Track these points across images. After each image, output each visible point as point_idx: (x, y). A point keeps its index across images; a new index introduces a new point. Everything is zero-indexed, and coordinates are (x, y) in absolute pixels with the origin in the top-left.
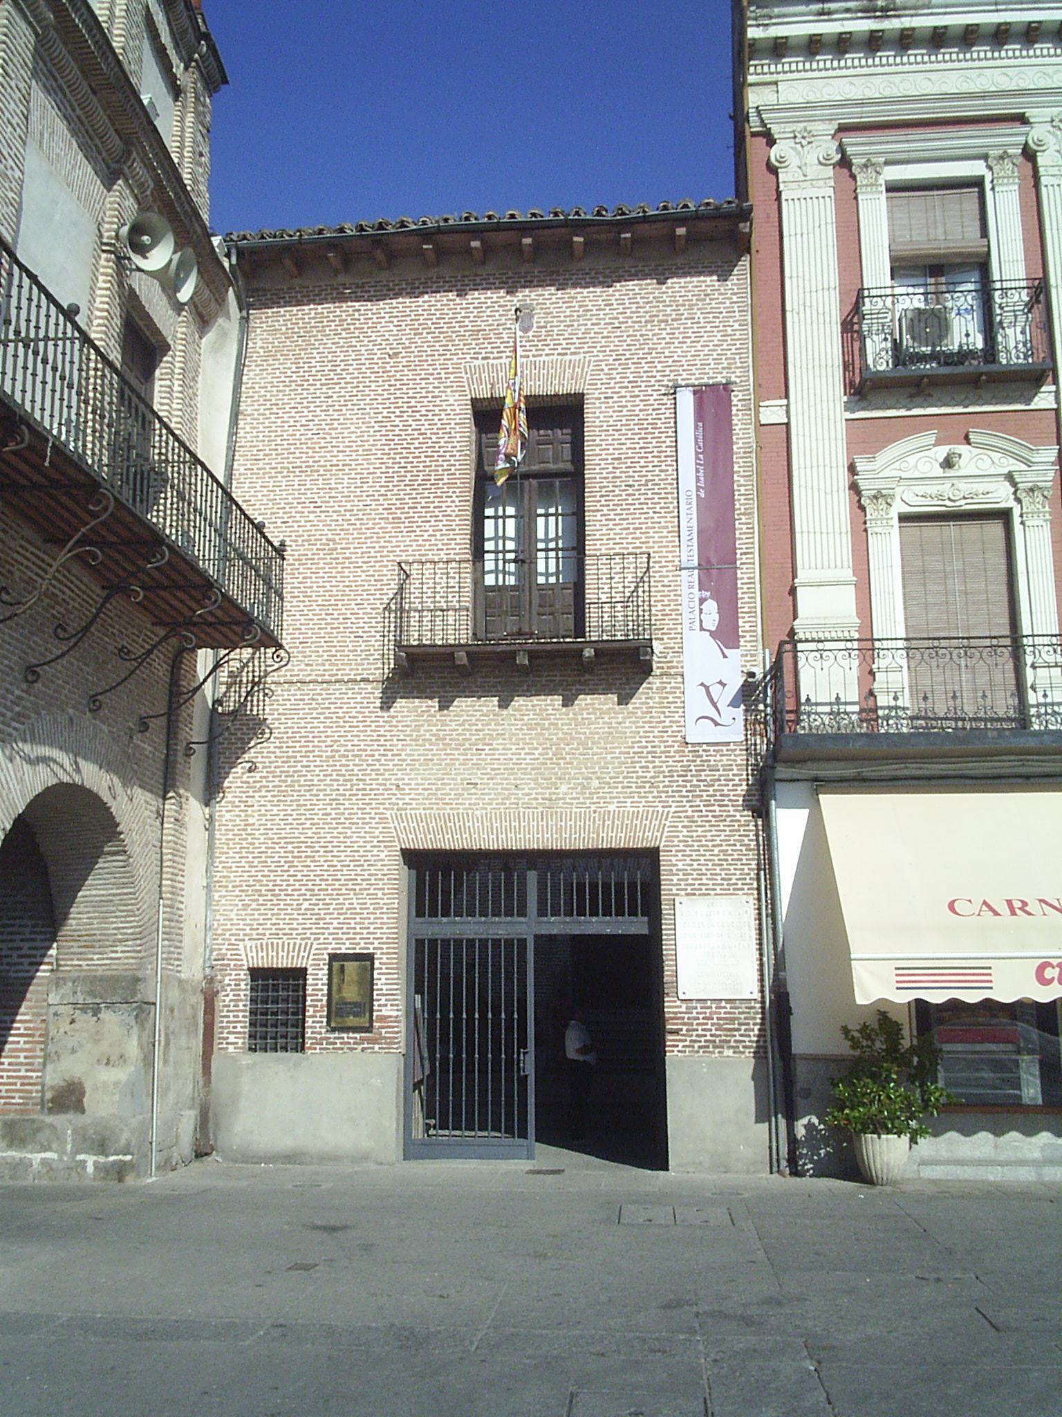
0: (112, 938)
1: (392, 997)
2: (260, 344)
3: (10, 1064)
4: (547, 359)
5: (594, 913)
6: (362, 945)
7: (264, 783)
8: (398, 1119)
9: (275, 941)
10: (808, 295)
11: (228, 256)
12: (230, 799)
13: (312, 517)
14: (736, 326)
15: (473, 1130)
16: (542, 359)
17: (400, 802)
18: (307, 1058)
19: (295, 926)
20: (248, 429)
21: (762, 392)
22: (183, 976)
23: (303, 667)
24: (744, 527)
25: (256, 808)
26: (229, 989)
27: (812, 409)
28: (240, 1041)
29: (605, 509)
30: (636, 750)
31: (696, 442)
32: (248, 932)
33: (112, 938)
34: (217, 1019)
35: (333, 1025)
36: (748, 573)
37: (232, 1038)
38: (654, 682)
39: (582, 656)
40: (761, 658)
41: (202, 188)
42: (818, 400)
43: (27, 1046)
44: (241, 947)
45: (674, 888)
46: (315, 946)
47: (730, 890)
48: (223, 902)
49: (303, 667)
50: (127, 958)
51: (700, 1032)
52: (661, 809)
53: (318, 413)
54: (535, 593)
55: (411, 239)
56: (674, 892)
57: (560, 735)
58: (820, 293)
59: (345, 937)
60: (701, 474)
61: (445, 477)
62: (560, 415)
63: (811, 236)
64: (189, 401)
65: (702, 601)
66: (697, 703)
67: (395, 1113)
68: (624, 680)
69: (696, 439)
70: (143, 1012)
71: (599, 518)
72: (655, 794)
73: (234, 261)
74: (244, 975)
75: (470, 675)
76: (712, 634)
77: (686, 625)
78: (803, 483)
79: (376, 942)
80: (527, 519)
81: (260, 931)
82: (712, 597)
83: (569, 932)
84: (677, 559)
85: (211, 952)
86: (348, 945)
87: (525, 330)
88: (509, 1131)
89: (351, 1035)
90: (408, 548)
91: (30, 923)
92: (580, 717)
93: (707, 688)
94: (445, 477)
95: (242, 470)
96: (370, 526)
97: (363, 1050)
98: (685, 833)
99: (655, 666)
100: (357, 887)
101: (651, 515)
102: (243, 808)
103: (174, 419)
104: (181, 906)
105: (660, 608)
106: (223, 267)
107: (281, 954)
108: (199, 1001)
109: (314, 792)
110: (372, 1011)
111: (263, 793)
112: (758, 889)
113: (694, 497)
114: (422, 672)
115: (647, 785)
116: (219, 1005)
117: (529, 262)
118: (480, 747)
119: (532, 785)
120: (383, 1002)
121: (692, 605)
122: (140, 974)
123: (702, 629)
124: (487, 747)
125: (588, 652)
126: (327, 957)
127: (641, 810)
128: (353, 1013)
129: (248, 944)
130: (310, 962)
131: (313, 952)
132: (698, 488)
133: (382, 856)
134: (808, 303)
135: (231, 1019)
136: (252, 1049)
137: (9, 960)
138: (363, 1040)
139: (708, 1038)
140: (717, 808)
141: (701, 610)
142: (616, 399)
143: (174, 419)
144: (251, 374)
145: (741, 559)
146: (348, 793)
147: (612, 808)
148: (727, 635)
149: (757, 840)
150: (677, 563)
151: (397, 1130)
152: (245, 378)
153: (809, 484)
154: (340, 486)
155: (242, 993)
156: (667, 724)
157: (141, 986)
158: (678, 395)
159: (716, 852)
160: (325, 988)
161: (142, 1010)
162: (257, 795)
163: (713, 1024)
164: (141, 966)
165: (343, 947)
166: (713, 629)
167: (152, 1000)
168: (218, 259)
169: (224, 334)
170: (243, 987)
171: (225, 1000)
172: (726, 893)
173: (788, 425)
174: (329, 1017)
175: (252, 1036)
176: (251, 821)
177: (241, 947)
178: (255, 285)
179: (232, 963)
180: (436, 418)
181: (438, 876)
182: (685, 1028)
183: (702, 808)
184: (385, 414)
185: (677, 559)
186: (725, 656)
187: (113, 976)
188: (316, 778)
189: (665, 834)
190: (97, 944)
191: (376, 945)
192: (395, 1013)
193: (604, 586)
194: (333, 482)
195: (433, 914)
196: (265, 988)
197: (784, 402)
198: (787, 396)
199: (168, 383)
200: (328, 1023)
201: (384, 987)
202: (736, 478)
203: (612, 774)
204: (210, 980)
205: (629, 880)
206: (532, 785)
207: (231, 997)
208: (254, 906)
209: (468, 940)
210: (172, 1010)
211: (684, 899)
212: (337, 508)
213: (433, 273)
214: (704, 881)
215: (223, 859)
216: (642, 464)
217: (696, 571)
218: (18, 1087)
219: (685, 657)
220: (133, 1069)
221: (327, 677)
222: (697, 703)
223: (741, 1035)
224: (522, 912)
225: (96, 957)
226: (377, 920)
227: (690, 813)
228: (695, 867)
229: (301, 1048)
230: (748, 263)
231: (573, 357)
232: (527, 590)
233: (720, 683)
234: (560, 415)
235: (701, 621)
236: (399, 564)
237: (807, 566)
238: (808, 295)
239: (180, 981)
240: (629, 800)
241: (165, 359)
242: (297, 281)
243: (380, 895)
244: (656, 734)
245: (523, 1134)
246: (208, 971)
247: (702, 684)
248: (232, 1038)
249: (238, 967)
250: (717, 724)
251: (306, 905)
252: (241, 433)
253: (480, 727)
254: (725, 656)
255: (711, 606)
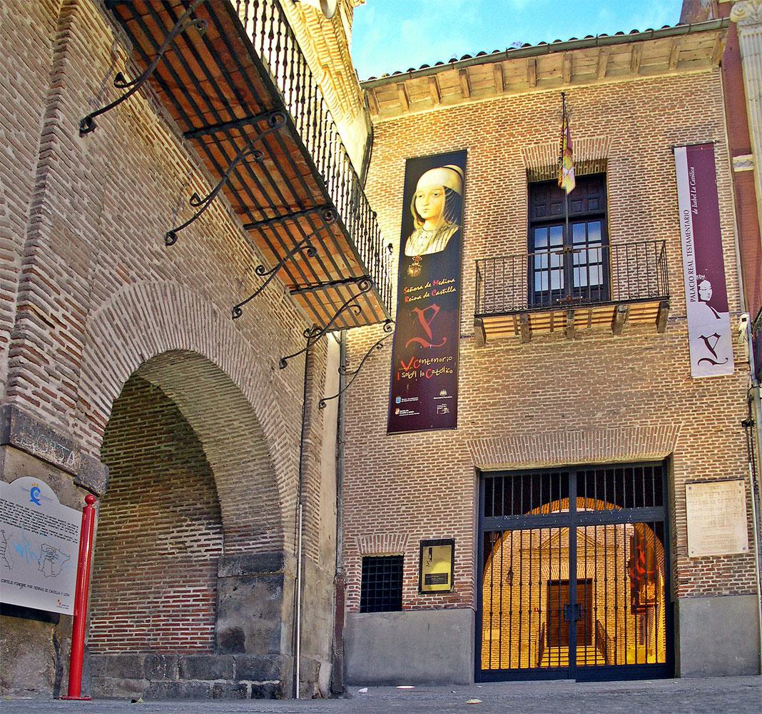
3: (193, 620)
31: (690, 180)
32: (361, 529)
43: (204, 608)
44: (356, 540)
46: (410, 537)
51: (705, 580)
52: (673, 425)
60: (695, 199)
65: (699, 282)
69: (690, 177)
76: (708, 303)
77: (688, 299)
79: (456, 531)
84: (679, 257)
86: (434, 535)
91: (205, 522)
93: (706, 340)
118: (536, 391)
121: (692, 284)
123: (700, 300)
129: (361, 537)
131: (408, 540)
132: (693, 209)
133: (461, 471)
137: (191, 549)
139: (711, 583)
141: (699, 288)
156: (677, 366)
160: (418, 565)
162: (369, 436)
163: (713, 574)
177: (356, 540)
179: (349, 551)
180: (502, 182)
182: (692, 578)
185: (679, 257)
186: (718, 317)
201: (462, 562)
208: (365, 511)
218: (199, 636)
223: (735, 580)
231: (599, 137)
233: (716, 335)
235: (699, 295)
243: (459, 498)
247: (702, 337)
250: (714, 363)
251: (403, 508)
255: (706, 285)
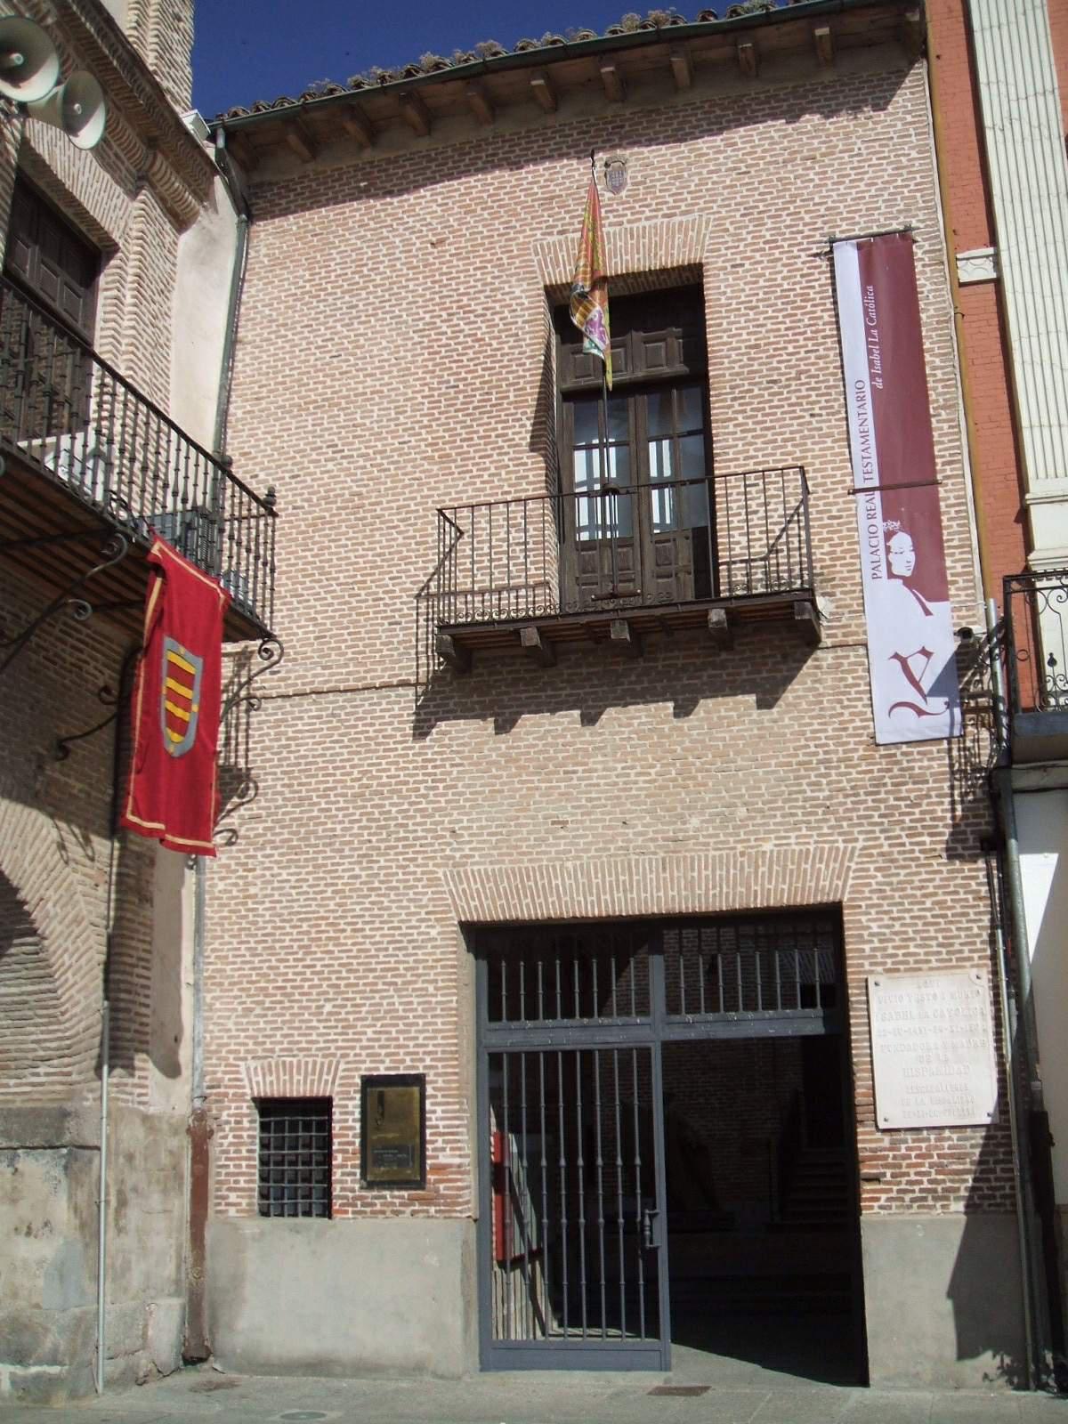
0: (30, 1055)
1: (453, 1134)
2: (264, 251)
4: (647, 224)
5: (750, 1005)
6: (408, 1063)
7: (269, 837)
8: (466, 1313)
9: (288, 1059)
10: (1014, 105)
11: (212, 138)
12: (224, 861)
13: (330, 466)
14: (914, 154)
15: (580, 1325)
16: (640, 224)
17: (458, 855)
18: (334, 1226)
19: (314, 1038)
20: (248, 361)
21: (955, 239)
22: (152, 1110)
23: (319, 670)
24: (945, 426)
25: (258, 872)
26: (227, 1128)
27: (1033, 255)
28: (244, 1202)
29: (740, 417)
30: (801, 758)
31: (866, 313)
32: (251, 1047)
33: (30, 1055)
34: (213, 1170)
35: (369, 1178)
36: (955, 491)
37: (233, 1197)
38: (825, 658)
39: (707, 622)
40: (982, 611)
41: (179, 58)
42: (1041, 243)
45: (866, 963)
46: (342, 1066)
47: (952, 961)
48: (218, 1005)
49: (319, 670)
50: (52, 1083)
52: (841, 845)
53: (339, 328)
54: (649, 547)
55: (451, 86)
56: (867, 967)
57: (687, 744)
58: (1032, 100)
59: (383, 1052)
60: (876, 357)
61: (511, 395)
62: (666, 304)
63: (1013, 27)
64: (154, 323)
65: (889, 535)
66: (888, 685)
67: (460, 1304)
68: (779, 658)
70: (76, 1160)
71: (731, 429)
72: (833, 823)
73: (221, 142)
74: (247, 1108)
75: (554, 665)
76: (908, 582)
77: (867, 572)
78: (1027, 357)
80: (633, 446)
81: (268, 1046)
82: (903, 529)
83: (712, 1035)
84: (848, 479)
85: (203, 1076)
86: (388, 1064)
87: (616, 189)
88: (633, 1328)
89: (396, 1193)
90: (458, 491)
92: (715, 716)
93: (904, 662)
94: (511, 395)
95: (239, 414)
96: (409, 469)
97: (413, 1213)
98: (880, 879)
99: (823, 633)
100: (399, 981)
101: (808, 419)
102: (241, 873)
103: (124, 341)
104: (143, 1010)
105: (827, 549)
106: (207, 157)
107: (296, 1077)
108: (184, 1144)
109: (337, 846)
110: (423, 1157)
111: (268, 851)
112: (994, 957)
113: (868, 390)
114: (484, 668)
115: (820, 811)
116: (214, 1151)
117: (616, 101)
119: (648, 820)
120: (439, 1144)
122: (68, 1106)
123: (891, 575)
124: (580, 769)
125: (717, 615)
126: (358, 1081)
127: (811, 848)
128: (397, 1157)
129: (252, 1064)
130: (337, 1089)
131: (340, 1074)
132: (872, 377)
133: (433, 933)
134: (1015, 114)
135: (232, 1170)
136: (265, 1213)
138: (412, 1200)
140: (927, 839)
141: (888, 550)
142: (747, 266)
143: (124, 341)
144: (253, 291)
145: (942, 471)
146: (383, 845)
147: (767, 847)
148: (928, 582)
149: (990, 884)
150: (849, 484)
151: (466, 1329)
152: (244, 297)
153: (1037, 359)
154: (367, 422)
155: (245, 1134)
156: (846, 717)
157: (71, 1123)
158: (836, 255)
159: (928, 904)
160: (358, 1125)
161: (76, 1156)
162: (259, 854)
164: (71, 1096)
165: (382, 1067)
166: (908, 574)
167: (95, 1142)
168: (198, 147)
169: (211, 241)
170: (246, 1124)
171: (222, 1143)
172: (945, 966)
173: (998, 283)
174: (364, 1167)
175: (264, 1195)
176: (253, 890)
177: (242, 1069)
178: (256, 178)
179: (231, 1091)
180: (497, 318)
181: (524, 961)
183: (905, 840)
184: (428, 320)
185: (848, 479)
186: (927, 613)
187: (33, 1110)
188: (339, 827)
189: (850, 882)
190: (13, 1064)
191: (428, 1062)
192: (457, 1161)
193: (744, 540)
194: (358, 416)
195: (514, 1016)
196: (280, 1127)
197: (991, 250)
198: (994, 241)
199: (115, 292)
200: (363, 1175)
201: (441, 1123)
202: (928, 357)
203: (767, 797)
204: (200, 1116)
205: (801, 946)
206: (648, 820)
207: (230, 1139)
208: (258, 1011)
209: (565, 1053)
210: (130, 1158)
211: (882, 979)
212: (364, 451)
213: (487, 132)
214: (912, 950)
215: (216, 945)
216: (791, 350)
217: (877, 494)
219: (869, 618)
220: (61, 1241)
221: (351, 683)
222: (888, 685)
224: (644, 1009)
225: (12, 1082)
226: (429, 1026)
227: (886, 849)
228: (897, 928)
229: (327, 1212)
230: (924, 71)
231: (684, 218)
232: (637, 544)
234: (666, 304)
235: (889, 565)
236: (440, 511)
237: (1042, 474)
238: (1014, 105)
239: (146, 1118)
240: (793, 835)
241: (113, 262)
242: (310, 167)
244: (830, 733)
245: (653, 1332)
246: (198, 1103)
247: (896, 656)
248: (233, 1197)
249: (239, 1097)
250: (920, 712)
251: (328, 1007)
252: (239, 366)
253: (569, 739)
254: (927, 613)
255: (903, 541)
